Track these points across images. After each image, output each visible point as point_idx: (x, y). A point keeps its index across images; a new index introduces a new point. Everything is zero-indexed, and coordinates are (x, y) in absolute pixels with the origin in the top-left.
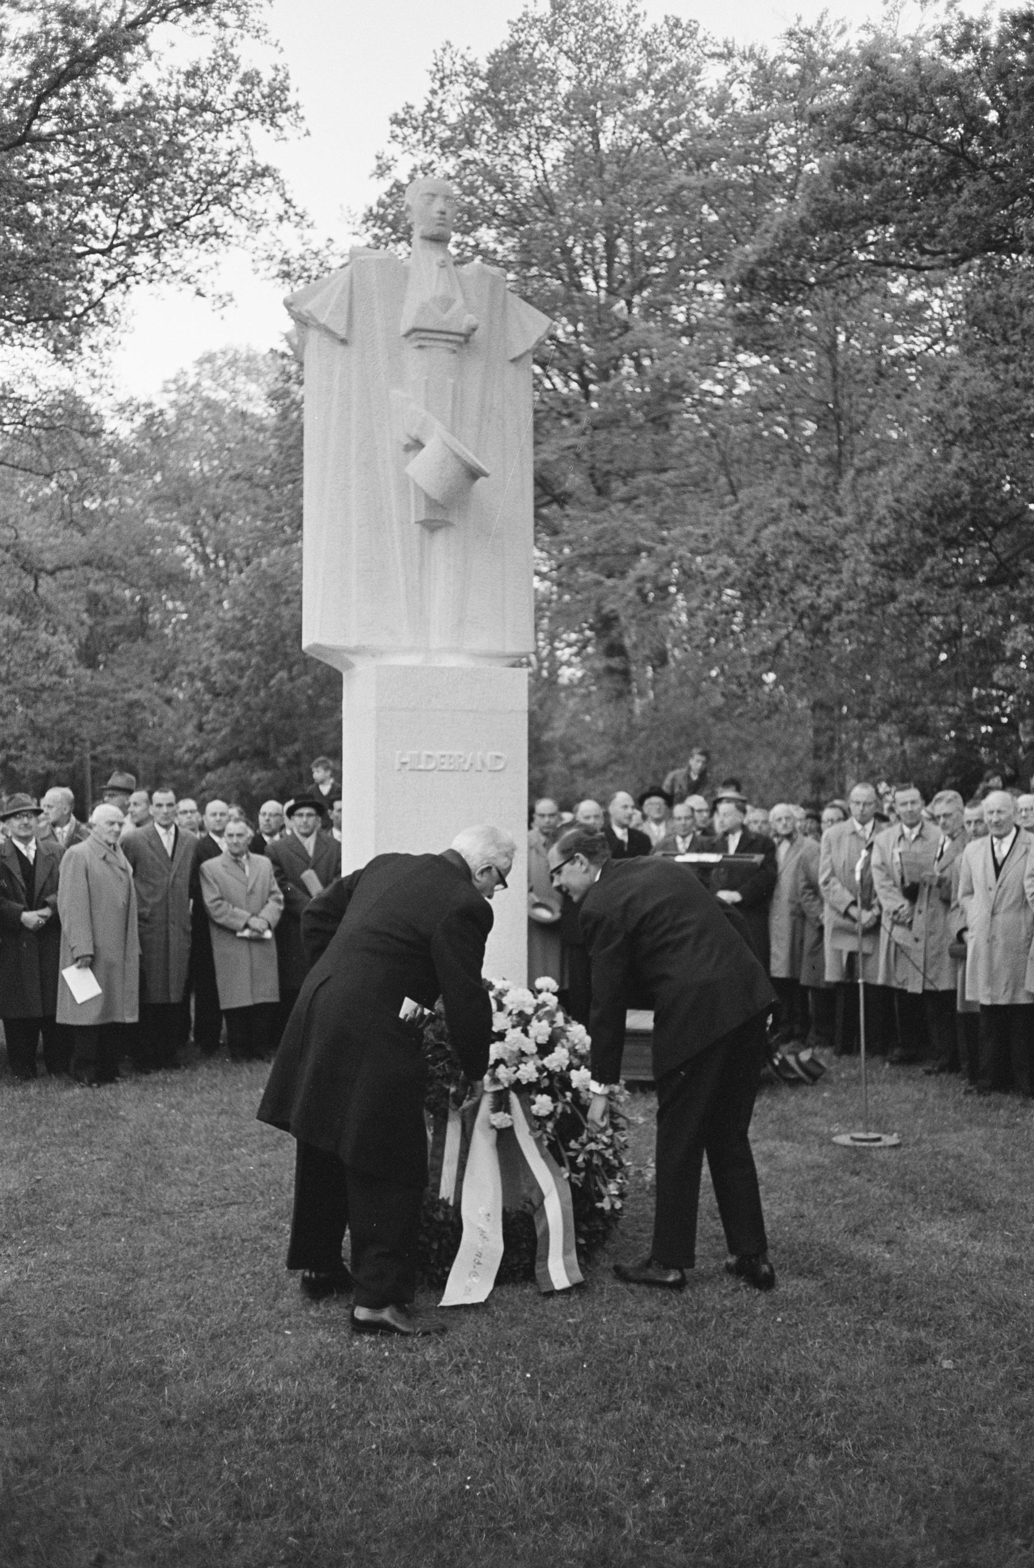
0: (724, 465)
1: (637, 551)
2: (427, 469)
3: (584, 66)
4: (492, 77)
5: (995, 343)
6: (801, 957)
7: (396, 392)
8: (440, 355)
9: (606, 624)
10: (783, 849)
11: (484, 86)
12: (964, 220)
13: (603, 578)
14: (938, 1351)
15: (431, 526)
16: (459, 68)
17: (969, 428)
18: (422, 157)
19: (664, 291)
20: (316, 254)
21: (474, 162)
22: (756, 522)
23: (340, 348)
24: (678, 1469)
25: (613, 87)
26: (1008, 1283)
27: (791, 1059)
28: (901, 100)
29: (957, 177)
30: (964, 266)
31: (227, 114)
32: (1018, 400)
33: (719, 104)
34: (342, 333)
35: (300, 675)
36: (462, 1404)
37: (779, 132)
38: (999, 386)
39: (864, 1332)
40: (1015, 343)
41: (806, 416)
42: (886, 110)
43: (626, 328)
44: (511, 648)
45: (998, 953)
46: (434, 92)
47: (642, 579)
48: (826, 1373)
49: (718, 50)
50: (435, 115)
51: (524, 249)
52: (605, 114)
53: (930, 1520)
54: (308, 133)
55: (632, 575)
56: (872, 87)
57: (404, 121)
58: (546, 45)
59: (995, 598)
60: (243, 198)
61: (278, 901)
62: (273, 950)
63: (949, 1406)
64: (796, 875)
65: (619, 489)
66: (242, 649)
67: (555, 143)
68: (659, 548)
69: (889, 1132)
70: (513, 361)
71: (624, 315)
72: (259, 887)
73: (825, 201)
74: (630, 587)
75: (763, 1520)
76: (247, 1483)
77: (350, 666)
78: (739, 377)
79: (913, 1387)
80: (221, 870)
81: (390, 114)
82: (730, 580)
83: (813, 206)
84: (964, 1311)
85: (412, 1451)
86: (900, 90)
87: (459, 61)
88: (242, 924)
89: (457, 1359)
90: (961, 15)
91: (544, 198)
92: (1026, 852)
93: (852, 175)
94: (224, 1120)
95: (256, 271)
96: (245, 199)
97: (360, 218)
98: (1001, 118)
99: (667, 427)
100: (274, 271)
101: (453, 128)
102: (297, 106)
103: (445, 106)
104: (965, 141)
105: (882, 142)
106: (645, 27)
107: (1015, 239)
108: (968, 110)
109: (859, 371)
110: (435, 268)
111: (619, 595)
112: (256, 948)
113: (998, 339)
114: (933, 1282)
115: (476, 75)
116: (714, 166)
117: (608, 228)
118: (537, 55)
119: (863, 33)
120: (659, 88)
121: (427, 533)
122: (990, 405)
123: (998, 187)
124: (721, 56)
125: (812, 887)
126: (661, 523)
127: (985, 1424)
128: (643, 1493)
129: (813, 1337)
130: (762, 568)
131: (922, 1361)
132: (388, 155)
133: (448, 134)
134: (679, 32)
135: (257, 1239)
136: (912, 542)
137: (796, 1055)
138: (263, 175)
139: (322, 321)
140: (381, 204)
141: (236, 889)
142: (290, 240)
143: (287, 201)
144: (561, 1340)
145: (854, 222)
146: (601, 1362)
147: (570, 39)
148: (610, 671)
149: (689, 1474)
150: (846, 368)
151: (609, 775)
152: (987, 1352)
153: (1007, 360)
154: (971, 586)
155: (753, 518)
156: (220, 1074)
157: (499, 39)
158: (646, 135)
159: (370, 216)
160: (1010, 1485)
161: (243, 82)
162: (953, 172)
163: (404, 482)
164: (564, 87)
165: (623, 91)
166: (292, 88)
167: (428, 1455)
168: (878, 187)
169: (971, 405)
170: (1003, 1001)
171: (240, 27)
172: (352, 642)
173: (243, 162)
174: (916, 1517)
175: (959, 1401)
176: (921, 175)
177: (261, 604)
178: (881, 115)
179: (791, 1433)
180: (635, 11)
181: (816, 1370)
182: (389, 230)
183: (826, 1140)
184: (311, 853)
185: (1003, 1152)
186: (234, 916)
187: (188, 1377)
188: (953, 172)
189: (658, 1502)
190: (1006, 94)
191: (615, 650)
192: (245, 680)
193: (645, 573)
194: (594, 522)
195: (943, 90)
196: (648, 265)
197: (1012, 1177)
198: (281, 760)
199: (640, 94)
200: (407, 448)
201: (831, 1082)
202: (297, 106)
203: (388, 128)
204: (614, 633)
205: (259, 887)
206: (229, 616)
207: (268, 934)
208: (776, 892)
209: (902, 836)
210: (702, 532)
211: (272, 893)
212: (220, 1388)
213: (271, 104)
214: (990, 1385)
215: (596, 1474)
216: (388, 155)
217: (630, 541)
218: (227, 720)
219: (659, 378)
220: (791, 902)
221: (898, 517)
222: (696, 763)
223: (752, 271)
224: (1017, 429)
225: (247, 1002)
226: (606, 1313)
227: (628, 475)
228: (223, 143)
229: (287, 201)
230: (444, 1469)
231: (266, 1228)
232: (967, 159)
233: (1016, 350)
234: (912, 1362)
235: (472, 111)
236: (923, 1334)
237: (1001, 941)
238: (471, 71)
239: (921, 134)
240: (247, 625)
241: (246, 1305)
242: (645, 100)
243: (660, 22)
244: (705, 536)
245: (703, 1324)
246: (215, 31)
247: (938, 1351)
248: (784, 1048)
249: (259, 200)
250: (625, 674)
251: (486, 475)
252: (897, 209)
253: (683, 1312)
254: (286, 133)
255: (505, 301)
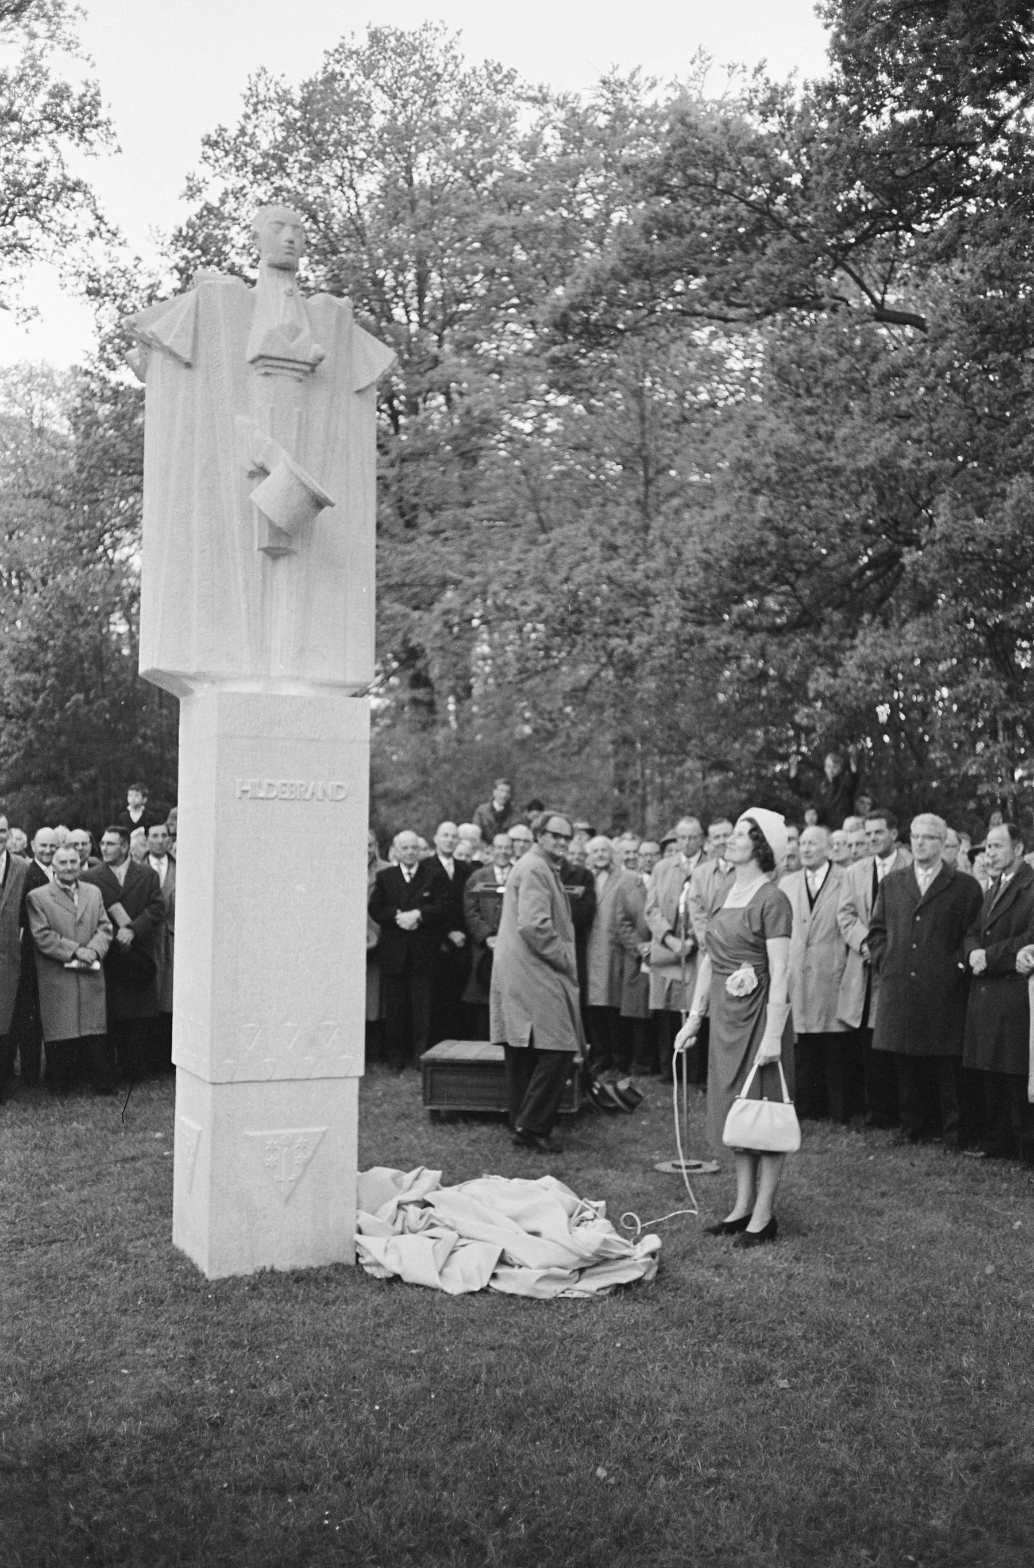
0: (534, 500)
1: (444, 583)
2: (272, 497)
3: (399, 102)
4: (305, 105)
5: (798, 395)
6: (620, 985)
7: (240, 418)
8: (286, 383)
9: (411, 655)
10: (601, 880)
11: (297, 114)
12: (766, 277)
13: (408, 610)
14: (773, 1372)
15: (274, 554)
16: (273, 95)
17: (775, 477)
18: (234, 181)
19: (473, 329)
20: (124, 272)
21: (289, 191)
22: (569, 560)
23: (184, 372)
24: (533, 1495)
25: (425, 123)
26: (833, 1304)
27: (609, 1088)
28: (710, 157)
29: (762, 234)
30: (769, 319)
31: (34, 126)
32: (820, 452)
33: (530, 148)
34: (187, 357)
35: (98, 697)
36: (311, 1439)
37: (589, 179)
38: (803, 437)
39: (701, 1354)
40: (818, 396)
41: (611, 457)
42: (696, 166)
43: (436, 361)
44: (352, 678)
45: (812, 984)
46: (247, 117)
47: (448, 612)
48: (669, 1396)
49: (531, 93)
50: (247, 139)
51: (335, 279)
52: (421, 150)
53: (781, 1535)
54: (119, 150)
55: (438, 608)
56: (683, 143)
57: (216, 143)
58: (362, 79)
59: (798, 644)
60: (53, 213)
61: (107, 931)
62: (102, 983)
63: (789, 1424)
64: (615, 905)
65: (427, 522)
66: (37, 671)
67: (368, 175)
68: (468, 581)
69: (709, 1159)
70: (358, 392)
71: (434, 350)
72: (88, 917)
73: (636, 251)
74: (437, 619)
75: (620, 1542)
76: (98, 1528)
77: (188, 692)
78: (541, 418)
79: (753, 1408)
80: (49, 899)
81: (202, 134)
82: (543, 616)
83: (624, 255)
84: (796, 1331)
85: (265, 1489)
86: (710, 148)
87: (272, 86)
88: (70, 954)
89: (302, 1393)
90: (768, 81)
91: (356, 230)
92: (839, 885)
93: (666, 226)
94: (39, 1156)
95: (63, 286)
96: (55, 213)
97: (169, 238)
98: (804, 181)
99: (475, 461)
100: (83, 288)
101: (265, 155)
102: (108, 122)
103: (258, 131)
104: (770, 200)
105: (692, 197)
106: (465, 68)
107: (817, 297)
108: (774, 172)
109: (665, 416)
110: (283, 297)
111: (426, 629)
112: (84, 981)
113: (801, 392)
114: (762, 1304)
115: (290, 102)
116: (527, 208)
117: (420, 262)
118: (353, 87)
119: (671, 89)
120: (474, 128)
121: (269, 560)
122: (795, 455)
123: (801, 247)
124: (534, 100)
125: (631, 919)
126: (470, 556)
127: (824, 1441)
128: (502, 1521)
129: (653, 1361)
130: (578, 608)
131: (759, 1381)
132: (199, 177)
133: (259, 161)
134: (497, 77)
135: (83, 1278)
136: (721, 588)
137: (614, 1084)
138: (74, 190)
139: (167, 343)
140: (190, 225)
141: (62, 915)
142: (98, 256)
143: (99, 218)
144: (406, 1370)
145: (665, 272)
146: (449, 1392)
147: (387, 74)
148: (415, 702)
149: (545, 1499)
150: (654, 413)
151: (413, 804)
152: (820, 1371)
153: (810, 411)
154: (776, 631)
155: (566, 557)
156: (30, 1110)
157: (313, 70)
158: (458, 174)
159: (179, 238)
160: (853, 1499)
161: (52, 95)
162: (758, 229)
163: (248, 508)
164: (379, 121)
165: (436, 129)
166: (104, 104)
167: (282, 1491)
168: (687, 239)
169: (777, 456)
170: (816, 1030)
171: (51, 37)
172: (192, 669)
173: (53, 175)
174: (768, 1533)
175: (799, 1419)
176: (729, 231)
177: (59, 625)
178: (692, 171)
179: (640, 1455)
180: (452, 52)
181: (658, 1393)
182: (198, 252)
183: (649, 1168)
184: (122, 882)
185: (819, 1177)
186: (61, 946)
187: (25, 1420)
188: (758, 229)
189: (517, 1529)
190: (809, 158)
191: (419, 680)
192: (40, 701)
193: (451, 606)
194: (403, 554)
195: (750, 150)
196: (459, 302)
197: (829, 1202)
198: (76, 786)
199: (454, 134)
200: (252, 475)
201: (648, 1110)
202: (108, 122)
203: (200, 148)
204: (420, 664)
205: (88, 917)
206: (24, 636)
207: (97, 966)
208: (596, 922)
209: (717, 869)
210: (515, 568)
211: (100, 923)
212: (59, 1431)
213: (81, 118)
214: (827, 1402)
215: (455, 1505)
216: (199, 177)
217: (439, 573)
218: (20, 744)
219: (468, 412)
220: (610, 931)
221: (707, 566)
222: (501, 791)
223: (564, 315)
224: (820, 480)
225: (74, 1034)
226: (449, 1343)
227: (433, 511)
228: (31, 154)
229: (99, 218)
230: (299, 1505)
231: (93, 1266)
232: (774, 219)
233: (819, 402)
234: (749, 1382)
235: (285, 139)
236: (758, 1354)
237: (815, 970)
238: (283, 98)
239: (728, 191)
240: (43, 646)
241: (78, 1346)
242: (460, 139)
243: (480, 65)
244: (518, 573)
245: (544, 1351)
246: (24, 40)
247: (773, 1372)
248: (601, 1077)
249: (75, 216)
250: (430, 706)
251: (332, 505)
252: (705, 262)
253: (524, 1340)
254: (96, 148)
255: (351, 333)
